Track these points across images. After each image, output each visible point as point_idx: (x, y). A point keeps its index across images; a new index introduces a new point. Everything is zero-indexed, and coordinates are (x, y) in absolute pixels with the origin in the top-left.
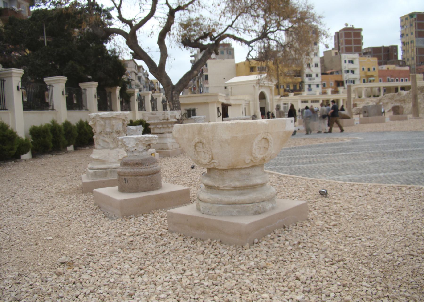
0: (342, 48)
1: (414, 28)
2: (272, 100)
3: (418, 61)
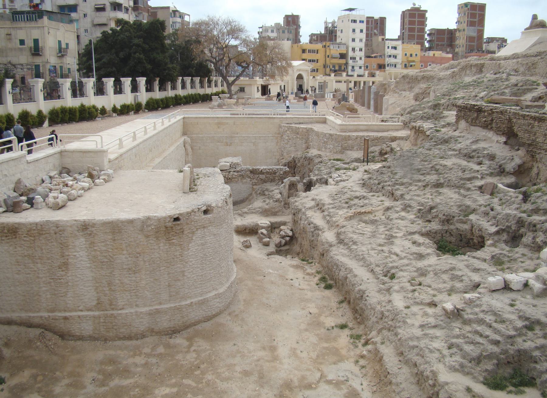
0: (406, 28)
1: (467, 17)
2: (308, 80)
3: (467, 48)
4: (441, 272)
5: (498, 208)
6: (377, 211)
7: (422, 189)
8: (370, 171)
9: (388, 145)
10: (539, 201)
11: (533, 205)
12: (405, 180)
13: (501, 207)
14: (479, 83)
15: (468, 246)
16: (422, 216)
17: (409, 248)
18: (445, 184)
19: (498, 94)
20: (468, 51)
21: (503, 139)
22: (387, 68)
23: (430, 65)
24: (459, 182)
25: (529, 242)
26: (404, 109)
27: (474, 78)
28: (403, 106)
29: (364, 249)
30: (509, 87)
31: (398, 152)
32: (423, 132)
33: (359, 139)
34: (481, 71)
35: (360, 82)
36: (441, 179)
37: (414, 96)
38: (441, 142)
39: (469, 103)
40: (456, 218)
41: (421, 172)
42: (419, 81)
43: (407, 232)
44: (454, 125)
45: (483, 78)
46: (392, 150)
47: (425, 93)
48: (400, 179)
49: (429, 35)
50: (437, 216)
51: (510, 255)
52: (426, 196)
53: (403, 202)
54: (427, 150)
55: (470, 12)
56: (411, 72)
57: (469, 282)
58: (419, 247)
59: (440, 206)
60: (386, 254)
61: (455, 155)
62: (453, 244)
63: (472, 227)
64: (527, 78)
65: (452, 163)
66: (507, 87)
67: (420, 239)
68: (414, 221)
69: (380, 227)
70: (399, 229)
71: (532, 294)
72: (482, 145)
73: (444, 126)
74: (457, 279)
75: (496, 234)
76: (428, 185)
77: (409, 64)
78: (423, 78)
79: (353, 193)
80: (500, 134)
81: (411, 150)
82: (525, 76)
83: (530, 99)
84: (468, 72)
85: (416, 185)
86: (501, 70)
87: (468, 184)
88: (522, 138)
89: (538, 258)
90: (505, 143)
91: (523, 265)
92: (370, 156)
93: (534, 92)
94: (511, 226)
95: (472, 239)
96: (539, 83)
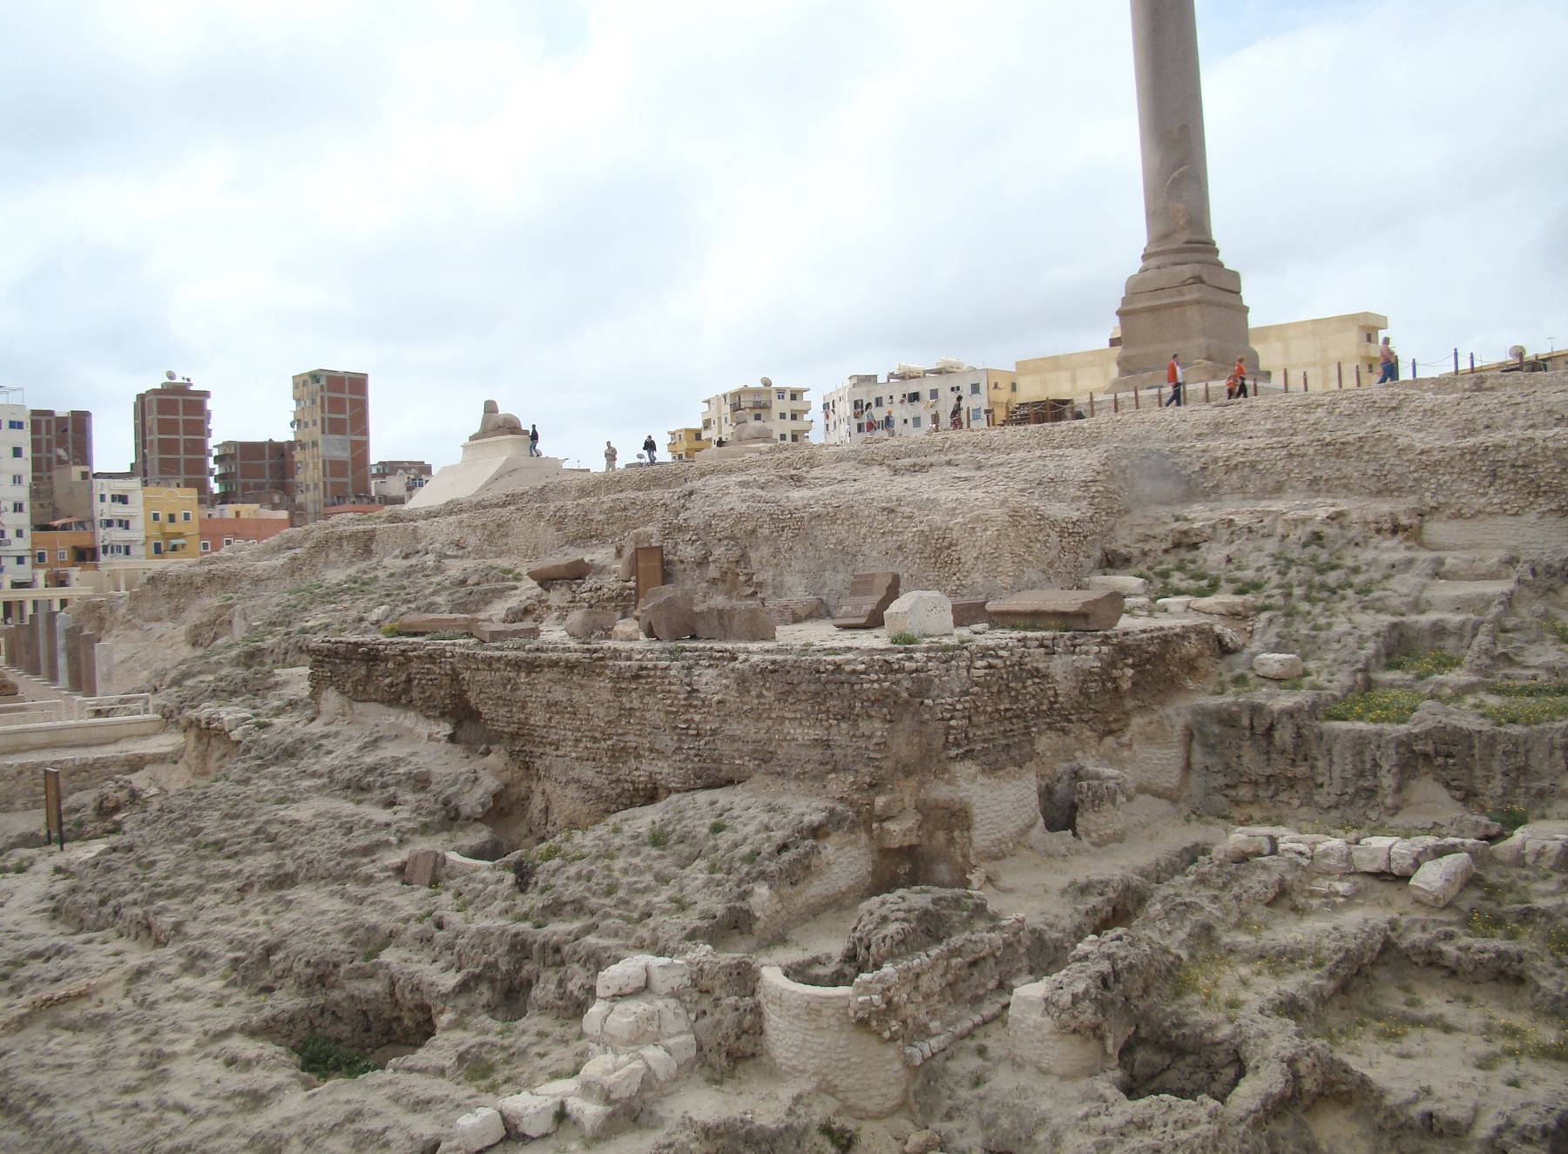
0: (151, 441)
4: (321, 1132)
5: (455, 919)
6: (108, 985)
7: (234, 898)
8: (73, 868)
9: (121, 783)
10: (559, 882)
11: (544, 896)
12: (182, 881)
13: (461, 915)
14: (364, 584)
15: (389, 1042)
16: (244, 978)
17: (218, 1082)
18: (301, 875)
19: (419, 609)
20: (329, 500)
21: (445, 729)
22: (103, 558)
23: (228, 543)
24: (338, 864)
25: (550, 997)
26: (164, 672)
27: (352, 571)
28: (158, 665)
29: (76, 1111)
30: (445, 588)
31: (153, 799)
32: (222, 734)
33: (28, 773)
34: (367, 552)
35: (21, 604)
36: (288, 861)
37: (189, 632)
38: (277, 758)
39: (343, 639)
40: (344, 968)
41: (227, 851)
42: (198, 590)
43: (206, 1033)
44: (306, 705)
45: (375, 569)
46: (134, 795)
47: (219, 622)
48: (167, 878)
49: (218, 459)
50: (288, 971)
51: (506, 1042)
52: (251, 917)
53: (182, 946)
54: (238, 782)
55: (327, 394)
56: (172, 565)
57: (408, 1144)
58: (248, 1071)
59: (293, 941)
60: (149, 1115)
61: (319, 789)
62: (346, 1043)
63: (393, 984)
64: (489, 562)
65: (312, 812)
66: (440, 590)
67: (248, 1048)
68: (223, 998)
69: (122, 1033)
70: (180, 1029)
71: (583, 1137)
72: (389, 751)
73: (279, 712)
74: (372, 1142)
75: (460, 992)
76: (251, 885)
77: (168, 544)
78: (210, 579)
79: (22, 944)
80: (434, 717)
81: (192, 790)
82: (484, 557)
83: (503, 615)
84: (333, 555)
85: (216, 891)
86: (420, 547)
87: (365, 864)
88: (492, 719)
89: (581, 1036)
90: (452, 739)
91: (545, 1062)
92: (68, 823)
93: (510, 596)
94: (497, 961)
95: (399, 1019)
96: (519, 574)
